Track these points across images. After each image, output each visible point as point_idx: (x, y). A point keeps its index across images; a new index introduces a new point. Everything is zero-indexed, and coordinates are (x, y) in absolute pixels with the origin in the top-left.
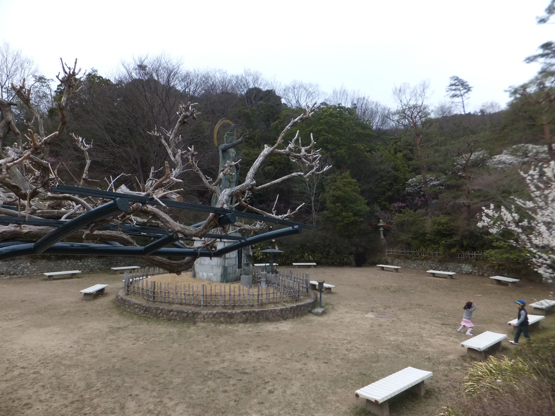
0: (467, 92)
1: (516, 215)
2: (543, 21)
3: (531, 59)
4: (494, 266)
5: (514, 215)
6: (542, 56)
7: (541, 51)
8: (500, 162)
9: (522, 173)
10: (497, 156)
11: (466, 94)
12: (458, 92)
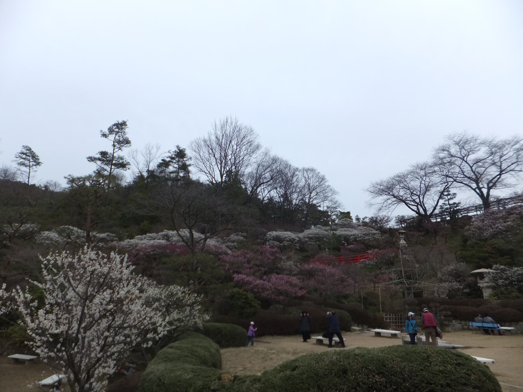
0: (35, 165)
1: (29, 295)
2: (104, 135)
3: (92, 159)
4: (16, 344)
5: (27, 295)
6: (99, 159)
7: (99, 156)
8: (48, 238)
9: (40, 257)
10: (47, 232)
11: (34, 167)
12: (27, 162)
